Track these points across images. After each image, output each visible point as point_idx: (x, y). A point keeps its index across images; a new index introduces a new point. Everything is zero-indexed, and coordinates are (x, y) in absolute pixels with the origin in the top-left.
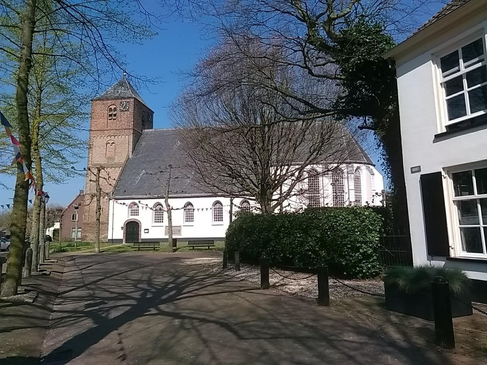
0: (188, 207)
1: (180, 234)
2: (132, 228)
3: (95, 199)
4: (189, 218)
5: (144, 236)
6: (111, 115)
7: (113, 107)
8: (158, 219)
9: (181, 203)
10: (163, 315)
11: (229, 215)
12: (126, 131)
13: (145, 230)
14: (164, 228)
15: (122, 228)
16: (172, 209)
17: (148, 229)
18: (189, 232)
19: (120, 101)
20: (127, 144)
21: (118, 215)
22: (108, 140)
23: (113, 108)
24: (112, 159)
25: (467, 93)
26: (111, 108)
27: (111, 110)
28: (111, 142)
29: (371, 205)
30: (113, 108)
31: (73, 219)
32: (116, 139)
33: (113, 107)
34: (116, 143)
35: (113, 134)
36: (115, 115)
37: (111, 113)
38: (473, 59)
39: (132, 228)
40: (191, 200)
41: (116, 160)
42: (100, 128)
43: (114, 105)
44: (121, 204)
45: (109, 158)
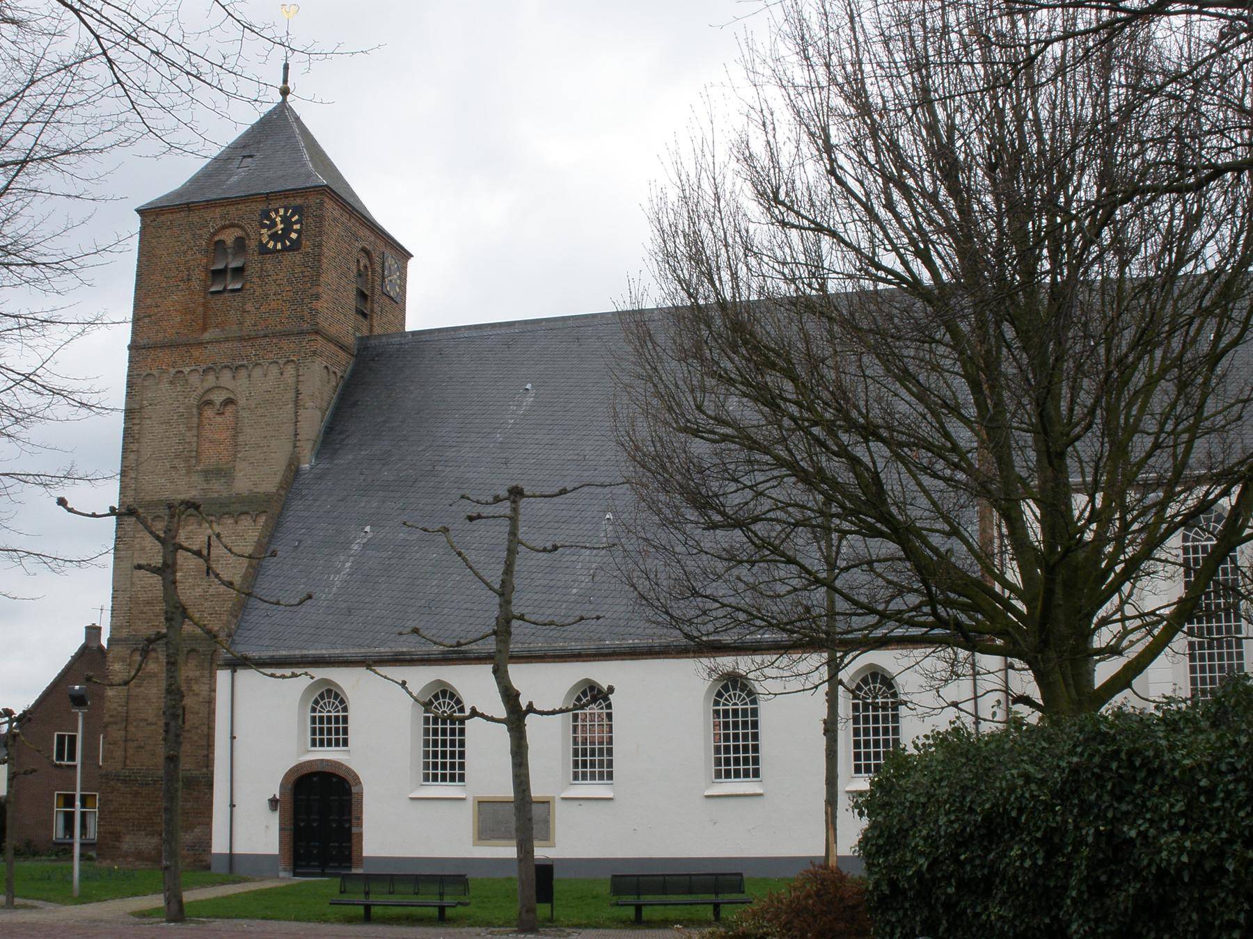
2: (320, 806)
3: (156, 665)
4: (593, 759)
6: (218, 274)
7: (229, 237)
8: (444, 754)
10: (309, 921)
11: (823, 741)
12: (284, 343)
15: (273, 803)
16: (474, 713)
18: (585, 832)
22: (207, 385)
24: (222, 473)
26: (223, 242)
28: (218, 397)
31: (60, 757)
32: (239, 386)
34: (242, 402)
35: (227, 362)
36: (239, 271)
37: (220, 266)
38: (80, 875)
39: (320, 806)
41: (243, 484)
43: (232, 226)
45: (208, 474)
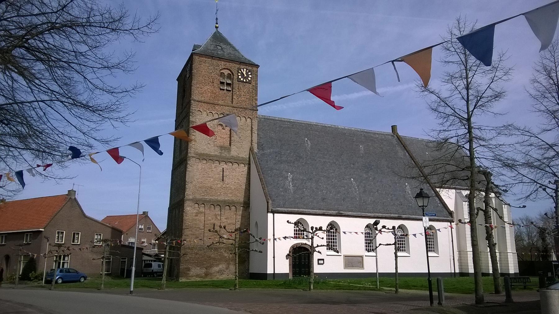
0: (333, 228)
1: (362, 267)
5: (317, 269)
7: (226, 72)
9: (323, 221)
13: (319, 260)
14: (342, 256)
17: (323, 260)
19: (238, 66)
20: (250, 132)
21: (280, 234)
23: (226, 74)
25: (61, 190)
27: (222, 75)
29: (252, 239)
30: (226, 74)
33: (226, 72)
39: (301, 257)
40: (339, 220)
42: (207, 100)
44: (520, 207)
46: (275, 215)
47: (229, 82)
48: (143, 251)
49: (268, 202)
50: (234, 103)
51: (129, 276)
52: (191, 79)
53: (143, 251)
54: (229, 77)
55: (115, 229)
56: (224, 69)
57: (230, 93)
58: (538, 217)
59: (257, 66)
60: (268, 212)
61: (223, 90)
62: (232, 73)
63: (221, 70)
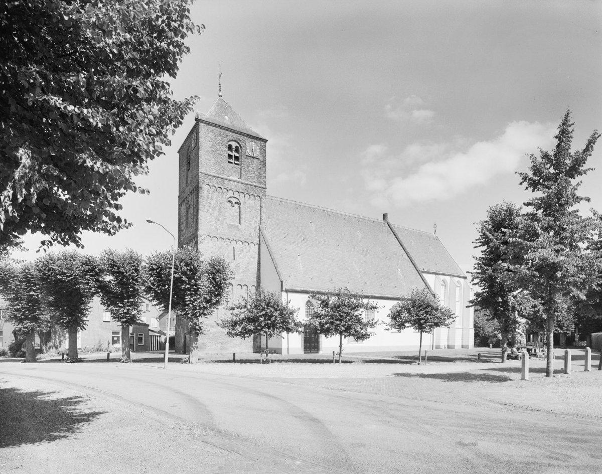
7: (234, 144)
23: (234, 147)
27: (230, 147)
33: (234, 144)
46: (232, 359)
47: (237, 155)
48: (149, 328)
49: (273, 361)
50: (242, 178)
51: (165, 349)
52: (198, 149)
53: (149, 328)
54: (237, 150)
55: (26, 271)
56: (232, 140)
57: (240, 167)
58: (34, 262)
59: (266, 141)
60: (282, 291)
61: (231, 163)
62: (240, 146)
63: (229, 141)
